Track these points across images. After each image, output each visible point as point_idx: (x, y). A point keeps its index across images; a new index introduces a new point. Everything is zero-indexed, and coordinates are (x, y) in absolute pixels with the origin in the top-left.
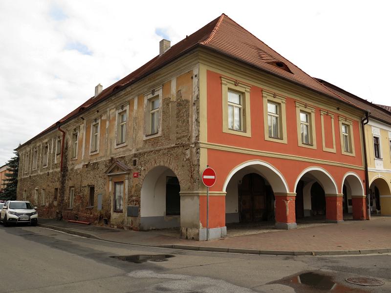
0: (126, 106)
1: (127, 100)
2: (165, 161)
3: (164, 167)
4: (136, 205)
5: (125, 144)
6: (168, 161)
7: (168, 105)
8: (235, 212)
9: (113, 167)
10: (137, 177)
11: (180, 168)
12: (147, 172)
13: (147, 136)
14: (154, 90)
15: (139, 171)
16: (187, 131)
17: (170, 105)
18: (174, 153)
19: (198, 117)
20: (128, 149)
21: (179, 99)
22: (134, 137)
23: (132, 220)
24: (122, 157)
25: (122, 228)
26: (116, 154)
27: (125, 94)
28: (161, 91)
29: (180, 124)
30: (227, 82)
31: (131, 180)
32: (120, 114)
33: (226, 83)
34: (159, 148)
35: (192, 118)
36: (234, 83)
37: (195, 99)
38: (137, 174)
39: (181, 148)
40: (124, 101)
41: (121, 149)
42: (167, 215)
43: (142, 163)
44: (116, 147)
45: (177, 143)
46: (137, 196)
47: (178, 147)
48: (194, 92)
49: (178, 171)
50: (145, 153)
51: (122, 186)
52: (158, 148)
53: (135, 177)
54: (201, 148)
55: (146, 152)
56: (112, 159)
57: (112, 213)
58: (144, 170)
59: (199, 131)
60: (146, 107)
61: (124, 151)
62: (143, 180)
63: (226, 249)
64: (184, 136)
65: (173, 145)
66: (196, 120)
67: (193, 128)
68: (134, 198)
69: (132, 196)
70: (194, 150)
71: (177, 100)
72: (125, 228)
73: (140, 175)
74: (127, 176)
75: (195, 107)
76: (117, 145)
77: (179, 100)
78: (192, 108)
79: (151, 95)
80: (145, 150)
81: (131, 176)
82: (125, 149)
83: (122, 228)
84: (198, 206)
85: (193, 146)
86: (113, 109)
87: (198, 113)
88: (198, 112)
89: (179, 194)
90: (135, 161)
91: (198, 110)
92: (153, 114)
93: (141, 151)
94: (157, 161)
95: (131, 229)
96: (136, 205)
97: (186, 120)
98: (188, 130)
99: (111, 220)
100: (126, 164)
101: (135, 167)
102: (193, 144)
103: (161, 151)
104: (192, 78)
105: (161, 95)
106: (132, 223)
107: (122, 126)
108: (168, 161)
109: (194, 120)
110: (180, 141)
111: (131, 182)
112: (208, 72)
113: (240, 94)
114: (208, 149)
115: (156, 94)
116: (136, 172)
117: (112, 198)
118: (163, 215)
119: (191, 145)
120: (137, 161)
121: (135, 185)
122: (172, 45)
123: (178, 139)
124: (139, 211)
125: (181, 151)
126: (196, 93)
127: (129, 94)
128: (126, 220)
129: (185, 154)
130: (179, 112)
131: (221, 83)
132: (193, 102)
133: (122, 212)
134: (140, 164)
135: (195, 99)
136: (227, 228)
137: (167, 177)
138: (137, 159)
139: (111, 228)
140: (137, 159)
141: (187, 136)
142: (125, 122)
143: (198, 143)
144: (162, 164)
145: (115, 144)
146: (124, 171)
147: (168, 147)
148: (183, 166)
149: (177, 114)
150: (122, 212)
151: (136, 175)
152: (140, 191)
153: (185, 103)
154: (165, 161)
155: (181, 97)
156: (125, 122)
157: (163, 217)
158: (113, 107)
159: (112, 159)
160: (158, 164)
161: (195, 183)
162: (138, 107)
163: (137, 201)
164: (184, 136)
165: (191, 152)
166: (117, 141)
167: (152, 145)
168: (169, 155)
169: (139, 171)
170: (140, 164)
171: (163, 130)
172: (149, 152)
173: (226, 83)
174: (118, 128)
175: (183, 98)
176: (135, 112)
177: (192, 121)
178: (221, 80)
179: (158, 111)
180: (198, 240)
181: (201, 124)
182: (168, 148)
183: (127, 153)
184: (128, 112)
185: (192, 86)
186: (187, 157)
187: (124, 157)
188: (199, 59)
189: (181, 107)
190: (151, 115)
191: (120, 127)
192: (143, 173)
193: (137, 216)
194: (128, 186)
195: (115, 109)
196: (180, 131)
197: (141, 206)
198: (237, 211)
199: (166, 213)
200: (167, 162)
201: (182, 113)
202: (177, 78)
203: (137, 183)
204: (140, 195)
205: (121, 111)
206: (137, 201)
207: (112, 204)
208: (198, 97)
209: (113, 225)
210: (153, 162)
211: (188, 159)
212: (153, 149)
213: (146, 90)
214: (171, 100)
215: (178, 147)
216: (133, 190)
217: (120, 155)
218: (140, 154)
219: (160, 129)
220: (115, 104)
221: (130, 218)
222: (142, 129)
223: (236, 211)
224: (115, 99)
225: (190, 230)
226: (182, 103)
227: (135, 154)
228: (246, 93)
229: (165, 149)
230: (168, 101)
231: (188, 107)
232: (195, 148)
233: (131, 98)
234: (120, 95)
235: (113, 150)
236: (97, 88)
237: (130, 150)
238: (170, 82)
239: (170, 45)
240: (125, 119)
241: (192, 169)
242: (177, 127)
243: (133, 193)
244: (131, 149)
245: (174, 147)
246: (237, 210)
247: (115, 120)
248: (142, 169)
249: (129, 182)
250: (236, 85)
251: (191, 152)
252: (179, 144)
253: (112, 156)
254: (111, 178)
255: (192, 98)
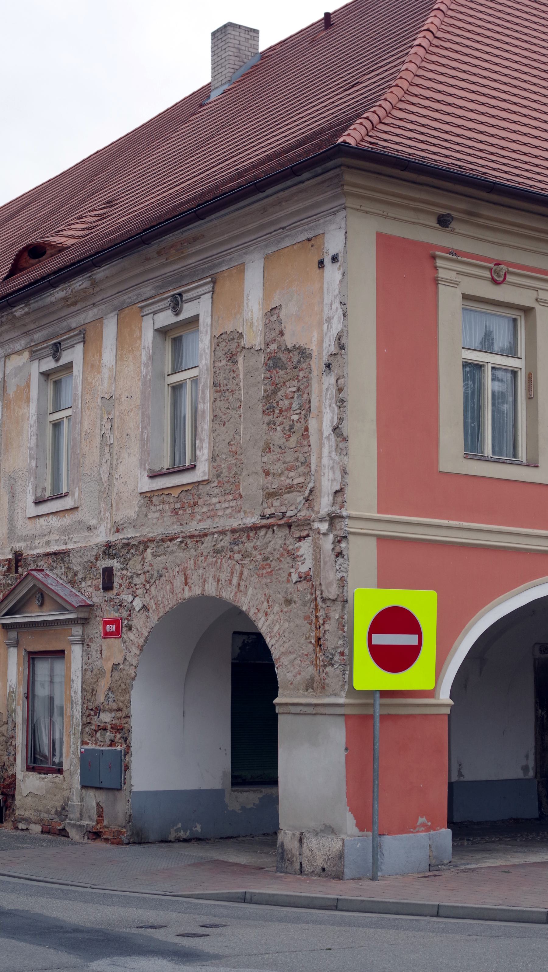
0: (72, 346)
1: (74, 322)
2: (223, 577)
3: (217, 601)
4: (112, 743)
5: (67, 503)
6: (235, 581)
7: (232, 358)
8: (520, 775)
9: (23, 591)
10: (117, 634)
11: (276, 608)
12: (154, 619)
13: (153, 476)
14: (180, 294)
15: (125, 614)
16: (301, 469)
17: (241, 359)
18: (255, 548)
19: (341, 420)
20: (80, 522)
21: (274, 341)
22: (105, 477)
23: (98, 804)
24: (55, 554)
25: (63, 833)
26: (33, 538)
27: (65, 299)
28: (206, 300)
29: (277, 437)
30: (459, 273)
31: (94, 646)
32: (46, 375)
33: (452, 276)
34: (201, 526)
35: (321, 423)
36: (487, 274)
37: (333, 349)
38: (118, 623)
39: (282, 533)
40: (64, 324)
41: (54, 521)
42: (234, 784)
43: (136, 580)
44: (33, 511)
45: (268, 512)
46: (119, 710)
47: (268, 527)
48: (329, 320)
49: (271, 617)
50: (145, 543)
51: (59, 666)
52: (194, 527)
53: (107, 635)
54: (350, 538)
55: (151, 540)
56: (18, 557)
57: (20, 776)
58: (145, 608)
59: (344, 472)
60: (152, 358)
61: (65, 531)
62: (141, 648)
63: (433, 906)
64: (290, 489)
65: (250, 521)
66: (336, 429)
67: (325, 460)
68: (106, 717)
69: (97, 710)
70: (327, 544)
71: (267, 345)
72: (74, 834)
73: (130, 628)
74: (77, 631)
75: (333, 380)
76: (38, 503)
77: (274, 347)
78: (320, 383)
79: (169, 312)
80: (149, 532)
81: (96, 629)
82: (67, 520)
83: (63, 833)
84: (343, 754)
85: (324, 527)
86: (18, 353)
87: (341, 403)
88: (342, 401)
89: (274, 706)
90: (108, 573)
91: (340, 390)
92: (177, 388)
93: (130, 533)
94: (194, 578)
95: (96, 835)
96: (112, 743)
97: (297, 426)
98: (306, 463)
99: (17, 802)
100: (72, 583)
101: (110, 594)
102: (322, 520)
103: (208, 542)
104: (321, 264)
105: (205, 320)
106: (100, 815)
107: (57, 425)
108: (235, 581)
109: (327, 429)
110: (276, 503)
111: (95, 655)
112: (379, 235)
113: (513, 313)
114: (380, 539)
115: (188, 312)
116: (113, 615)
117: (20, 716)
118: (218, 786)
119: (316, 525)
120: (117, 574)
121: (108, 666)
122: (263, 45)
123: (271, 495)
124: (127, 768)
125: (280, 542)
126: (336, 327)
127: (84, 299)
128: (76, 801)
129: (294, 557)
130: (275, 392)
131: (436, 281)
132: (325, 359)
133: (60, 771)
134: (131, 585)
135: (333, 349)
136: (455, 836)
137: (235, 633)
138: (115, 564)
139: (18, 833)
140: (115, 564)
141: (302, 486)
142: (68, 412)
143: (342, 517)
144: (211, 589)
145: (30, 499)
146: (65, 609)
147: (235, 523)
148: (288, 602)
149: (268, 397)
150: (60, 771)
151: (111, 628)
152: (127, 691)
153: (296, 359)
154: (223, 577)
155: (282, 334)
156: (68, 412)
157: (217, 794)
158: (18, 346)
159: (18, 557)
160: (197, 591)
161: (329, 669)
162: (119, 357)
163: (117, 729)
164: (290, 489)
165: (317, 549)
166: (36, 487)
167: (175, 512)
168: (237, 557)
169: (125, 614)
170: (131, 585)
171: (213, 459)
172: (163, 540)
173: (452, 276)
174: (40, 435)
175: (289, 341)
176: (106, 374)
177: (320, 431)
178: (436, 268)
179: (195, 380)
180: (339, 877)
181: (353, 444)
182: (233, 531)
183: (76, 536)
184: (77, 369)
185: (322, 298)
186: (303, 569)
187: (67, 553)
188: (345, 194)
189: (281, 373)
190: (168, 392)
191: (49, 429)
192: (138, 622)
193: (119, 790)
194: (84, 671)
195: (26, 355)
196: (278, 467)
197: (133, 749)
198: (531, 774)
199: (234, 777)
200: (230, 581)
201: (286, 396)
202: (267, 258)
203: (118, 659)
204: (128, 707)
205: (49, 364)
206: (117, 729)
207: (20, 740)
208: (343, 341)
209: (27, 821)
210: (179, 581)
211: (306, 578)
212: (176, 529)
213: (147, 291)
214: (246, 342)
215: (268, 527)
216: (103, 685)
217: (48, 543)
218: (127, 545)
219: (204, 454)
220: (26, 333)
221: (91, 793)
222: (135, 448)
223: (525, 769)
224: (27, 314)
225: (312, 843)
226: (284, 357)
227: (109, 546)
228: (537, 307)
229: (223, 533)
230: (233, 346)
231: (308, 378)
232: (331, 537)
233: (90, 315)
234: (53, 299)
235: (20, 522)
236: (131, 755)
237: (89, 529)
238: (241, 269)
239: (256, 46)
240: (66, 399)
241: (321, 613)
242: (267, 449)
243: (101, 698)
244: (93, 522)
245: (255, 528)
246: (531, 763)
247: (28, 400)
248: (138, 604)
249: (86, 654)
250: (496, 282)
251: (317, 549)
252: (272, 515)
253: (19, 546)
254: (13, 634)
255: (321, 343)
